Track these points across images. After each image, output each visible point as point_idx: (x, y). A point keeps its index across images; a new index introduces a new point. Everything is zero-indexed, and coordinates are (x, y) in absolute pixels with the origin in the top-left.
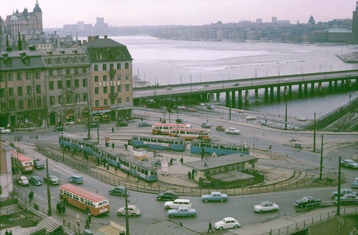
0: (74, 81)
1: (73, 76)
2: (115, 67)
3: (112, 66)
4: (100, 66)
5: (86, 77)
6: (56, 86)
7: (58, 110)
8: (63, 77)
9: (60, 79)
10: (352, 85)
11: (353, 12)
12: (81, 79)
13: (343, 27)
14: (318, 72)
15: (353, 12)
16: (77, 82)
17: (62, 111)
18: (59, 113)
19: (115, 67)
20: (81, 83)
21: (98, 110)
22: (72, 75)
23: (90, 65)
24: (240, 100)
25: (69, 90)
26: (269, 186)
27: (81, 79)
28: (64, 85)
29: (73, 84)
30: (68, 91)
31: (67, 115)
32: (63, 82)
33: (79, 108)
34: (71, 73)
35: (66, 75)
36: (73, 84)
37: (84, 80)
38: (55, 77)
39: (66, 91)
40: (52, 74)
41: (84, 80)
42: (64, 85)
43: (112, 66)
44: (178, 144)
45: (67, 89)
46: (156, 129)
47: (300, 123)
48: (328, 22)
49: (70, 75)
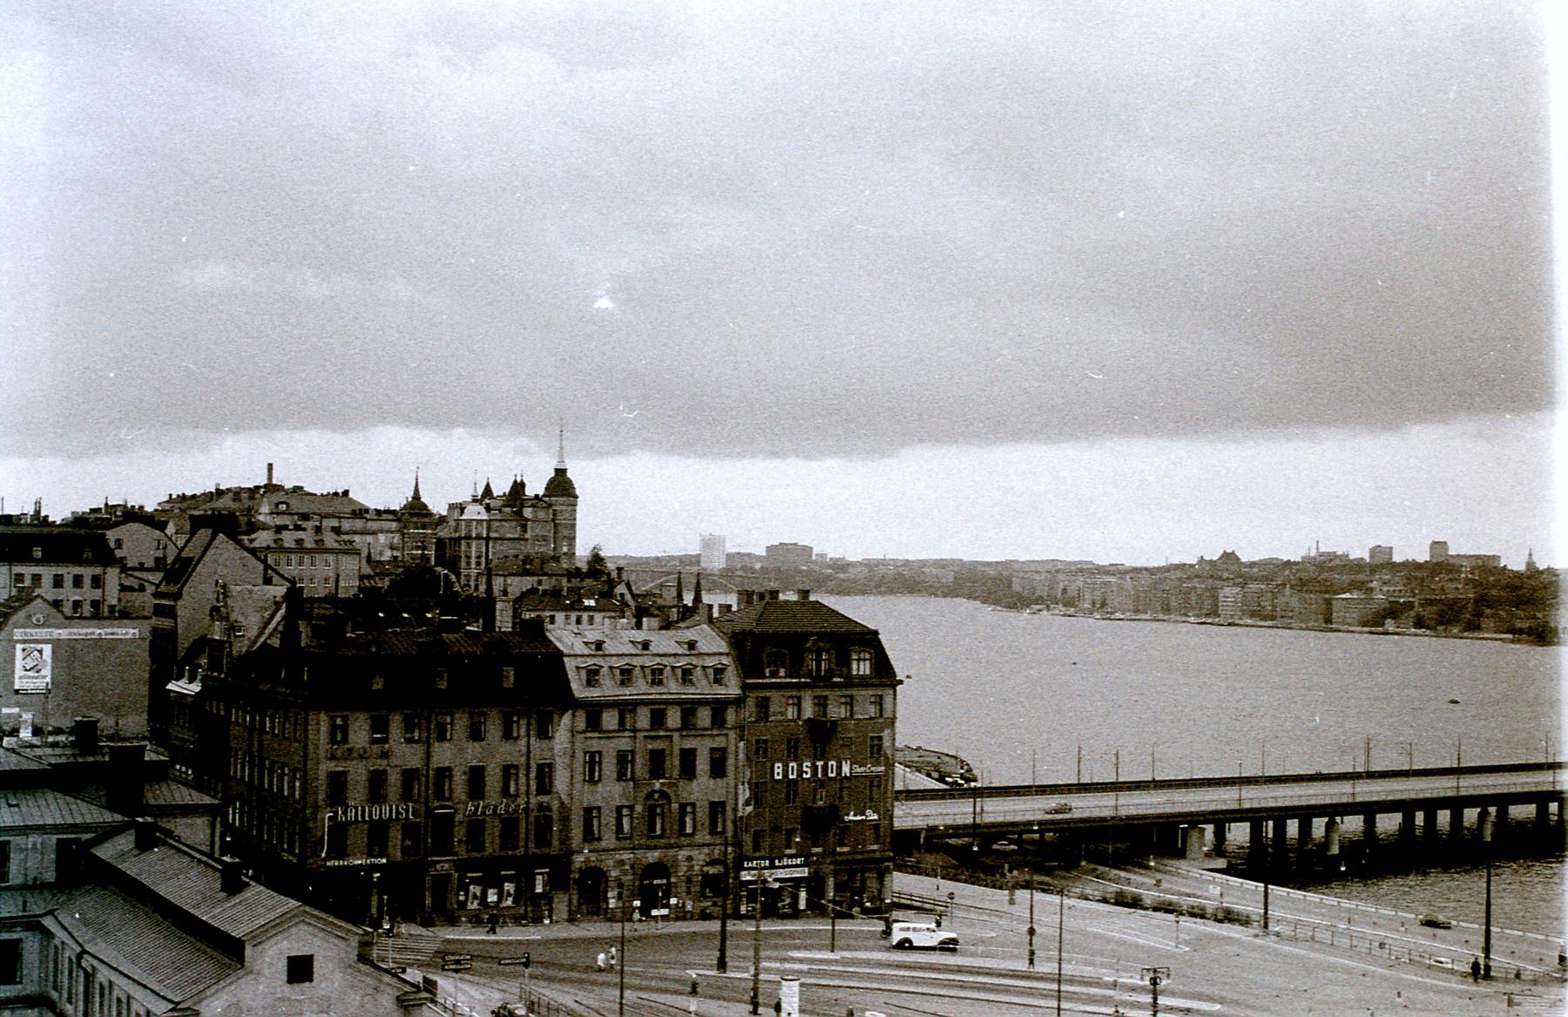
0: (676, 752)
1: (676, 735)
16: (688, 757)
20: (702, 764)
25: (657, 786)
27: (702, 749)
30: (654, 792)
33: (690, 859)
42: (641, 767)
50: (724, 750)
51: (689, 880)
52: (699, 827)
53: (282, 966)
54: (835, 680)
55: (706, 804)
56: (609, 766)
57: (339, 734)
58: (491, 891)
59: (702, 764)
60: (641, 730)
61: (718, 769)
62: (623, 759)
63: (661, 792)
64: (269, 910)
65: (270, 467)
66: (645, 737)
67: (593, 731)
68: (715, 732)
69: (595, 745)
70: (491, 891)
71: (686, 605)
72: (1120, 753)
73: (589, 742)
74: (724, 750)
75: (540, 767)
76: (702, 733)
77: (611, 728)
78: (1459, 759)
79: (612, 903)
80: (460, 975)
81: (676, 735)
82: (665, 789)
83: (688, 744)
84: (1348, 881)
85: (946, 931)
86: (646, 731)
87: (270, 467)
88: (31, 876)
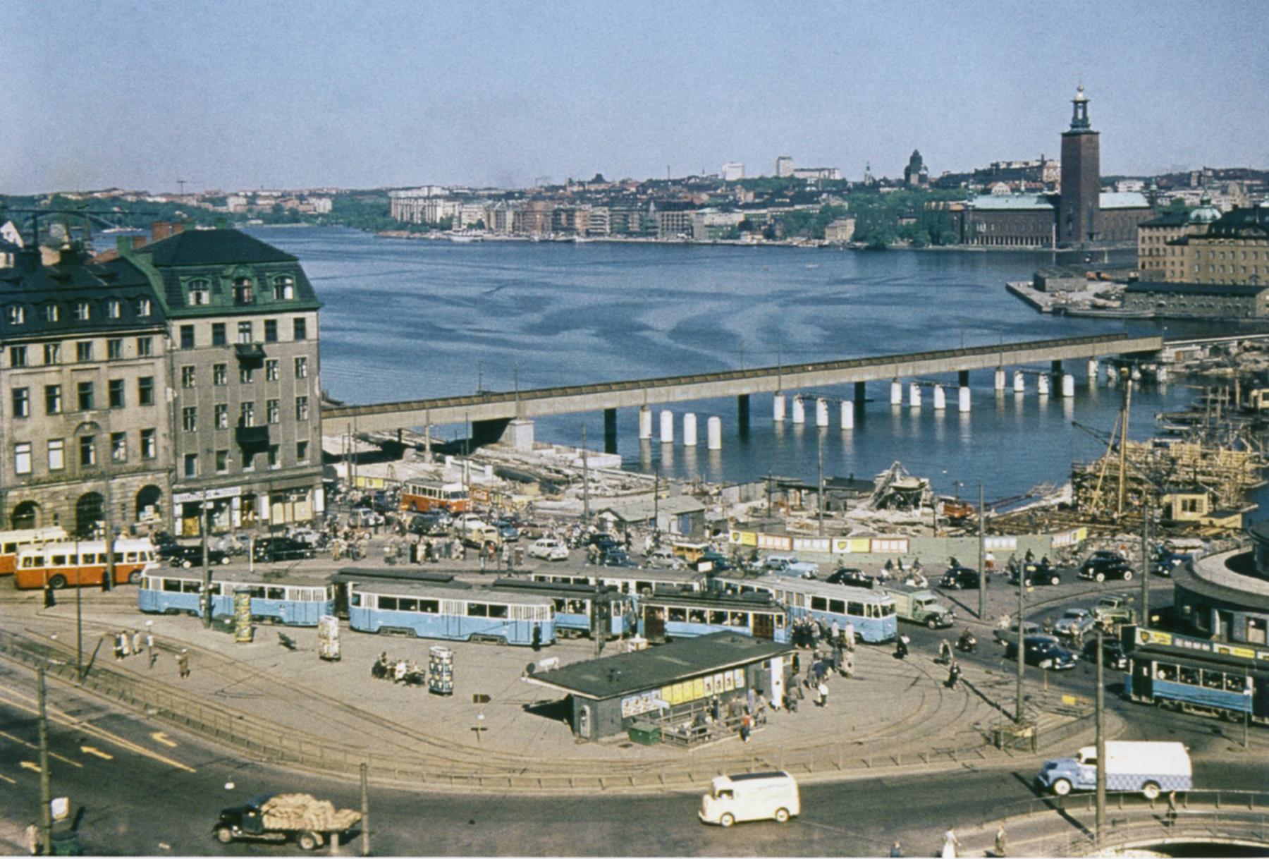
0: (106, 385)
3: (246, 329)
4: (203, 331)
5: (150, 368)
11: (1064, 135)
14: (756, 176)
15: (1064, 135)
16: (116, 388)
17: (62, 498)
18: (49, 505)
19: (259, 336)
20: (131, 393)
23: (893, 475)
24: (679, 450)
29: (101, 395)
30: (84, 423)
31: (376, 514)
35: (78, 363)
36: (101, 395)
39: (76, 423)
40: (22, 361)
42: (69, 400)
44: (469, 605)
45: (82, 417)
46: (81, 564)
49: (92, 362)
51: (124, 506)
52: (130, 454)
53: (51, 608)
54: (55, 319)
56: (37, 400)
57: (113, 349)
59: (131, 393)
61: (145, 395)
62: (51, 393)
63: (91, 423)
65: (789, 158)
66: (73, 370)
68: (142, 361)
69: (22, 382)
72: (1141, 222)
73: (15, 379)
76: (128, 362)
77: (70, 361)
81: (103, 367)
83: (115, 375)
84: (91, 531)
85: (588, 414)
87: (789, 158)
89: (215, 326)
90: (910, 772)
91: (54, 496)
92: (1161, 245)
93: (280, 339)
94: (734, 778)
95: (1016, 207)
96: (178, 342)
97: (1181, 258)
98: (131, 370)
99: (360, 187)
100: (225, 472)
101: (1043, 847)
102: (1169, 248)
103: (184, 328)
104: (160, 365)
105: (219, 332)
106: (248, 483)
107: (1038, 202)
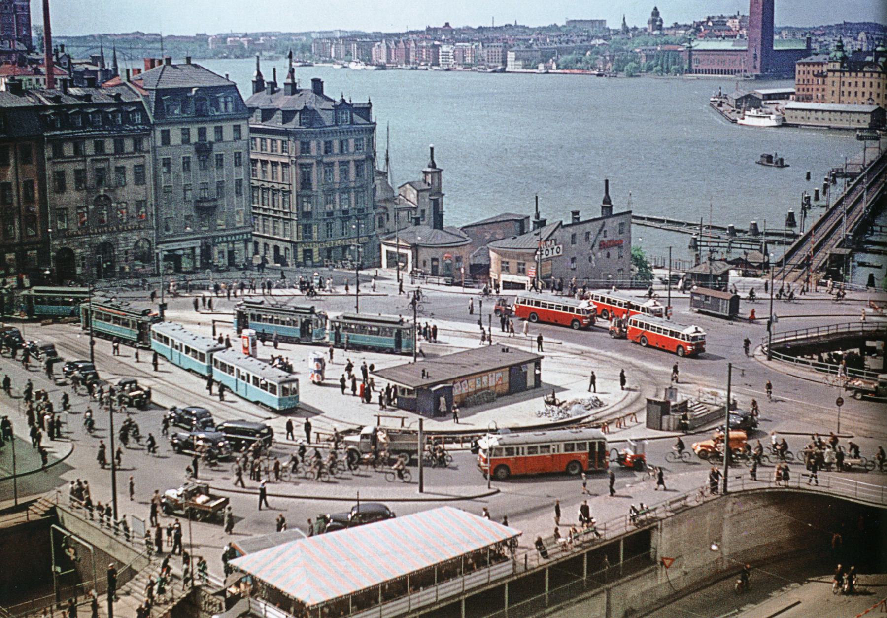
0: (113, 169)
1: (111, 158)
2: (211, 136)
3: (202, 132)
5: (142, 159)
6: (70, 182)
7: (77, 244)
8: (89, 159)
9: (80, 167)
10: (276, 262)
12: (70, 169)
13: (727, 36)
21: (233, 242)
22: (108, 155)
25: (102, 192)
26: (507, 573)
27: (129, 164)
28: (90, 180)
30: (100, 196)
32: (89, 175)
33: (125, 239)
34: (107, 151)
37: (77, 172)
38: (69, 160)
41: (77, 172)
42: (90, 180)
43: (202, 132)
45: (98, 191)
47: (835, 309)
48: (641, 21)
50: (142, 166)
55: (134, 202)
58: (880, 360)
60: (89, 156)
62: (80, 176)
63: (105, 196)
64: (472, 436)
67: (58, 157)
70: (880, 360)
71: (107, 70)
74: (142, 166)
75: (26, 183)
78: (387, 160)
79: (79, 270)
80: (81, 349)
82: (108, 194)
83: (59, 168)
86: (92, 156)
88: (47, 450)
89: (216, 127)
90: (553, 432)
91: (81, 245)
92: (810, 77)
93: (172, 143)
94: (59, 486)
95: (706, 48)
96: (159, 143)
97: (842, 89)
98: (130, 161)
99: (107, 33)
100: (171, 232)
101: (451, 506)
102: (815, 79)
103: (163, 131)
104: (149, 157)
105: (186, 133)
106: (206, 238)
107: (733, 45)
